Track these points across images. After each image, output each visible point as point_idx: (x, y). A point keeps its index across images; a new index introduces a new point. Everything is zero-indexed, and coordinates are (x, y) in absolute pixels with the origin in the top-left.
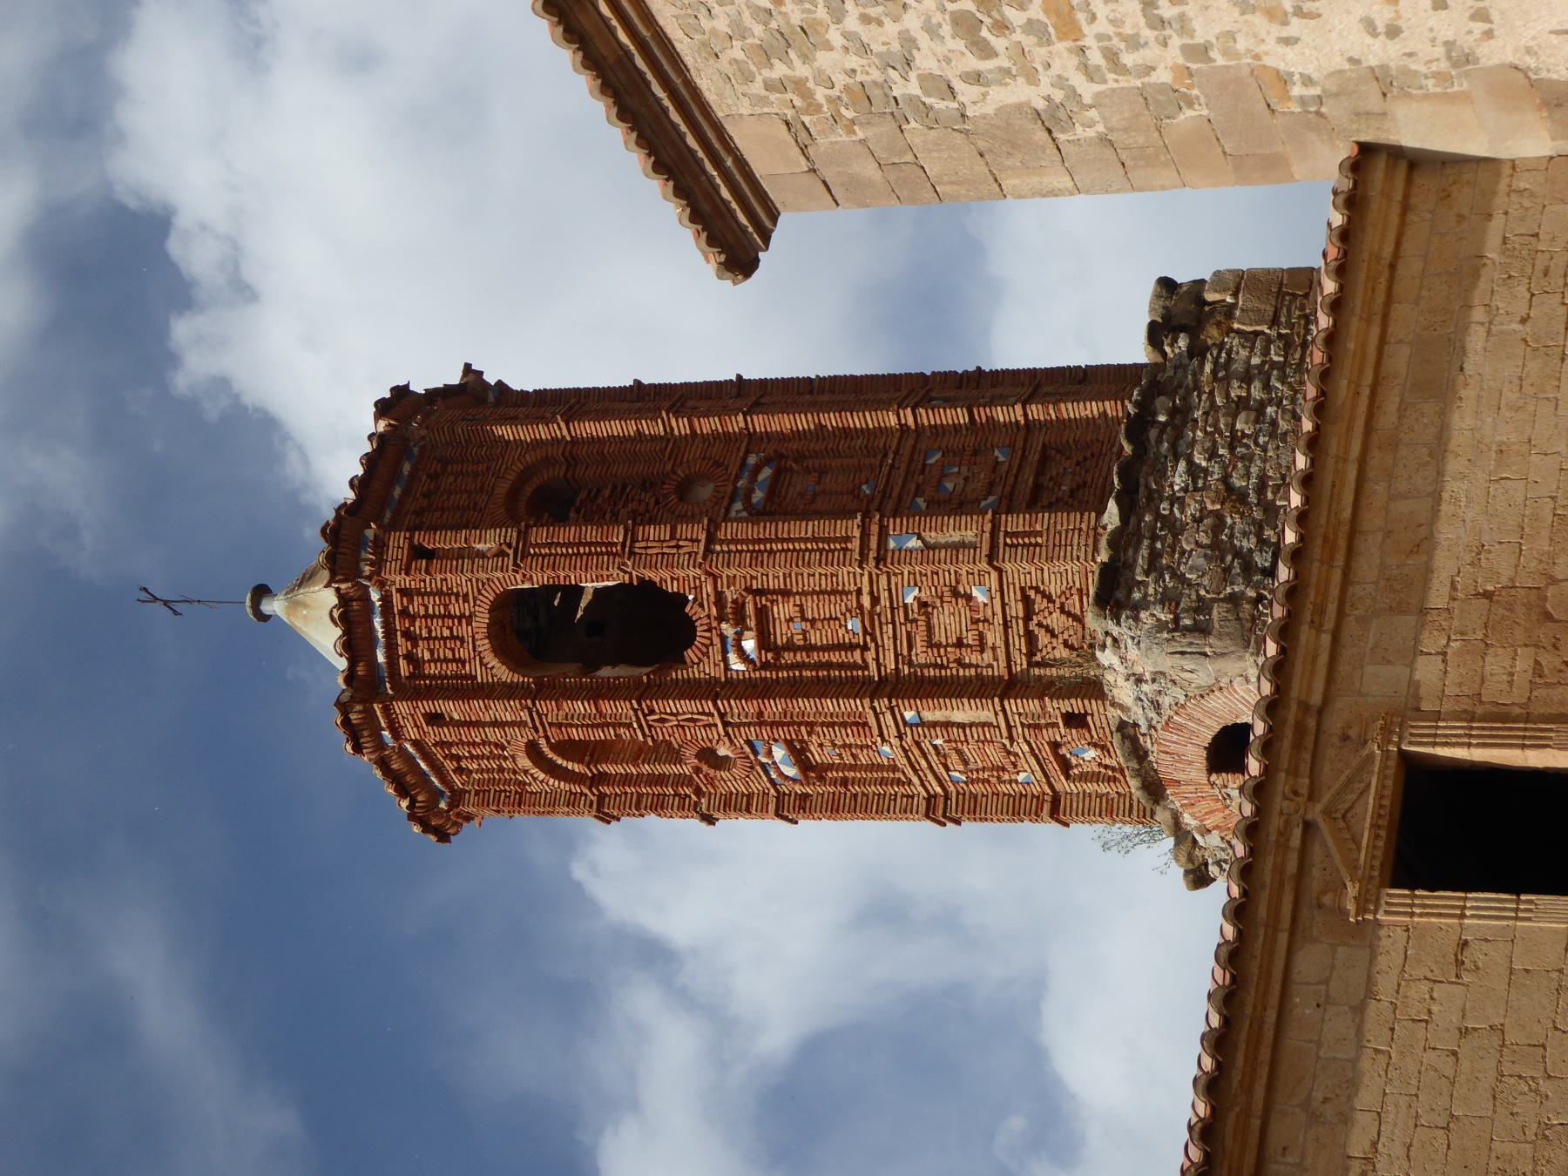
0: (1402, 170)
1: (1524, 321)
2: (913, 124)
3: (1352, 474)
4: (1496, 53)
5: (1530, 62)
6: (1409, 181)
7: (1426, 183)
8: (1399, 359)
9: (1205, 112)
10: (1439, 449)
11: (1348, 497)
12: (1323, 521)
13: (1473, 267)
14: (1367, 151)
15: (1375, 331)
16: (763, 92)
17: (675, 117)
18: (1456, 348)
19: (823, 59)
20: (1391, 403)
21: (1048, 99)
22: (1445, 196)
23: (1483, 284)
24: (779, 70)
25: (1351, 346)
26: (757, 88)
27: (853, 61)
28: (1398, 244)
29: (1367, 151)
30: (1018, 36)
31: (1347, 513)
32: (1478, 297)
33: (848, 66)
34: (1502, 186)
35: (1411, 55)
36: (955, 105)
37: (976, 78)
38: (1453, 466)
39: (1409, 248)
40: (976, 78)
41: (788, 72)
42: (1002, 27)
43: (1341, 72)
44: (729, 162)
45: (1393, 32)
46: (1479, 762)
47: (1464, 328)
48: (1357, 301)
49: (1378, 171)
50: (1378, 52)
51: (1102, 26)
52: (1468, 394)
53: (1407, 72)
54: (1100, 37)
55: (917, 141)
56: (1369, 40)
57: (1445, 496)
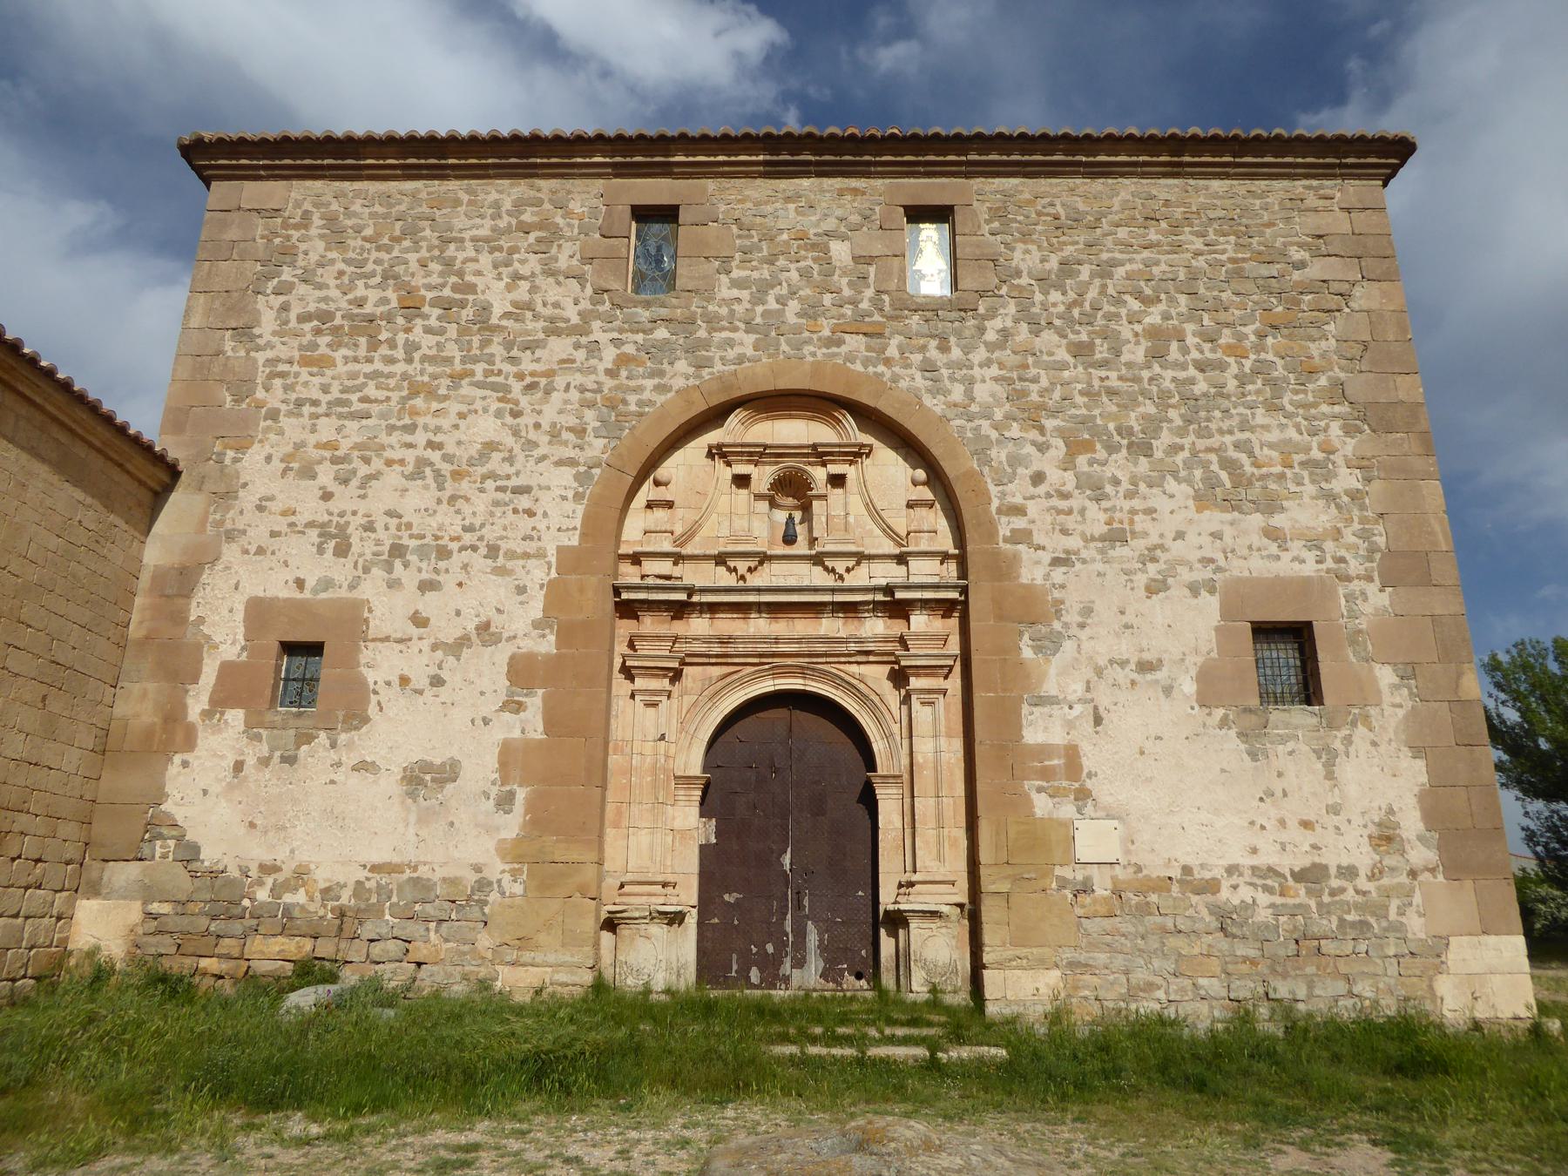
0: (158, 488)
1: (80, 522)
2: (259, 268)
3: (38, 400)
4: (230, 553)
5: (219, 567)
6: (151, 489)
7: (146, 497)
8: (80, 451)
9: (227, 406)
10: (34, 452)
11: (28, 393)
12: (24, 372)
13: (110, 508)
14: (174, 473)
15: (97, 443)
16: (304, 208)
17: (307, 162)
18: (77, 483)
19: (321, 245)
20: (63, 437)
21: (260, 336)
22: (140, 504)
23: (100, 508)
24: (317, 221)
25: (99, 428)
26: (307, 206)
27: (314, 257)
28: (128, 472)
29: (174, 473)
30: (309, 337)
31: (21, 388)
32: (95, 503)
33: (311, 254)
34: (137, 534)
35: (241, 512)
36: (269, 291)
37: (285, 308)
38: (24, 457)
39: (125, 478)
40: (285, 308)
41: (315, 225)
42: (318, 332)
43: (238, 478)
44: (262, 173)
45: (260, 508)
46: (791, 417)
47: (85, 490)
48: (118, 442)
49: (165, 478)
50: (248, 499)
51: (304, 377)
52: (55, 479)
53: (228, 509)
54: (297, 375)
55: (248, 264)
56: (258, 496)
57: (10, 446)
